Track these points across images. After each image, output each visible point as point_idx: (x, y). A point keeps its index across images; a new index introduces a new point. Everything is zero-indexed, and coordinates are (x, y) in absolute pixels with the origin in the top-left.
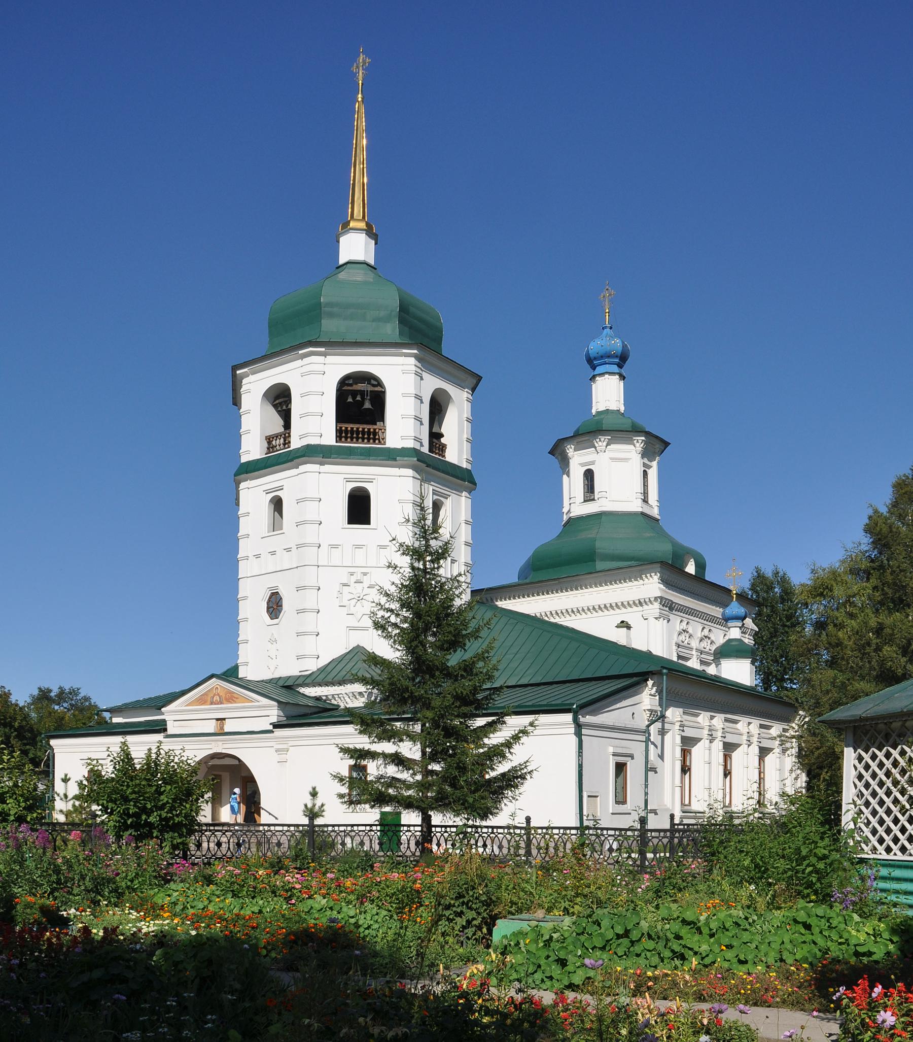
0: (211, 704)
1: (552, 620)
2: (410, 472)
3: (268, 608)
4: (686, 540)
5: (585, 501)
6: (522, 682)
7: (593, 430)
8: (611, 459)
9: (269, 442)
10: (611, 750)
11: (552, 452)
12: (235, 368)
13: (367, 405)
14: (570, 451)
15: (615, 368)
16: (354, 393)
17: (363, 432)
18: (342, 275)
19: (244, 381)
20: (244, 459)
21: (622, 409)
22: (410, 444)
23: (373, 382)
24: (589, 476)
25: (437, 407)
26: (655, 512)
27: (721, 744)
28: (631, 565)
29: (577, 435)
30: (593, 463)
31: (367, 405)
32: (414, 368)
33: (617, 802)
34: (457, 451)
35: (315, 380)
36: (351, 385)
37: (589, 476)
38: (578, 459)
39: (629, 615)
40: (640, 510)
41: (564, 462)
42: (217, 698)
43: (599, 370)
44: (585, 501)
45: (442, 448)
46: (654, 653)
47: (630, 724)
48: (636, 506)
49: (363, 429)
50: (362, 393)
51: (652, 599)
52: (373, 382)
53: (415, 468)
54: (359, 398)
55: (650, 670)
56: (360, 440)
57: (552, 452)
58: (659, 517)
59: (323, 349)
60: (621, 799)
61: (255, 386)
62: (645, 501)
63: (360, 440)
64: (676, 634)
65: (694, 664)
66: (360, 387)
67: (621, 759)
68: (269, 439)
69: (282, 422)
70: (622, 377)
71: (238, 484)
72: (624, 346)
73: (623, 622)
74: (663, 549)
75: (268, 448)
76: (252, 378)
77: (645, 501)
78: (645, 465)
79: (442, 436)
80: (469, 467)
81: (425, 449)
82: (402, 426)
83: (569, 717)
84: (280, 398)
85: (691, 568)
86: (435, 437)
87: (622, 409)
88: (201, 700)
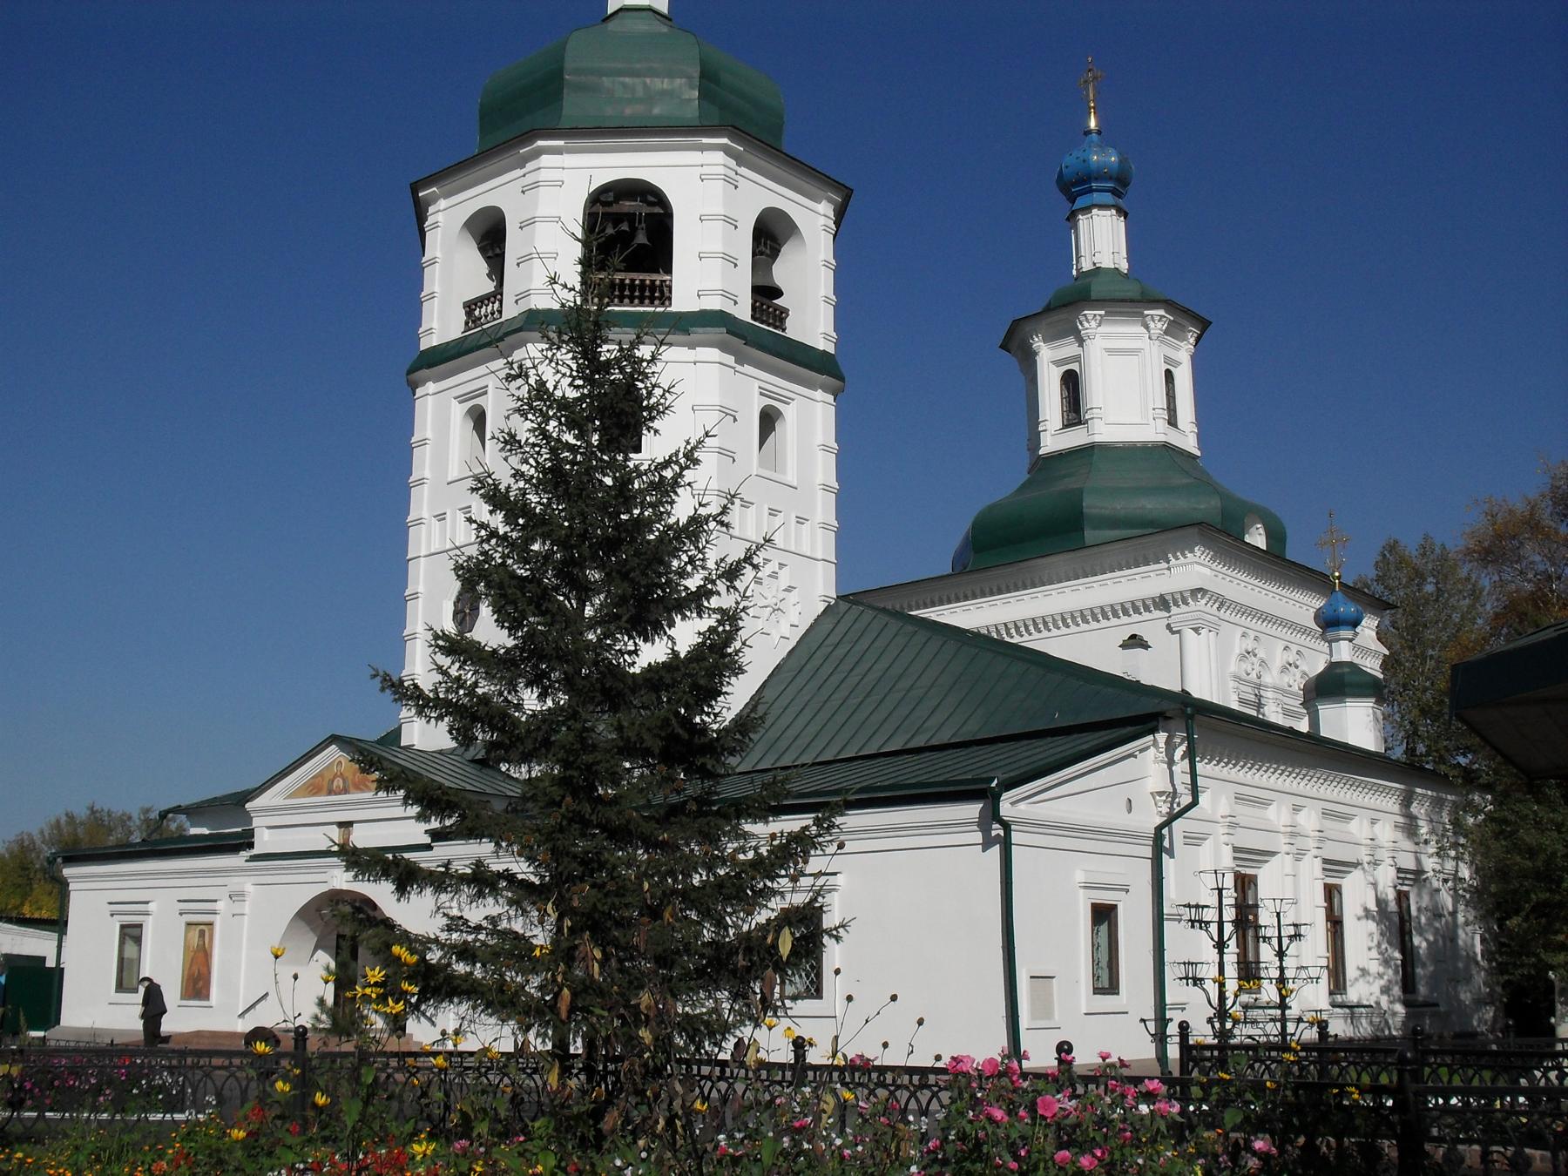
0: (330, 793)
1: (1016, 640)
2: (714, 354)
3: (456, 613)
4: (1244, 491)
5: (1065, 426)
6: (934, 742)
7: (1074, 298)
8: (1107, 350)
9: (469, 313)
10: (1080, 877)
11: (1004, 346)
12: (415, 188)
13: (641, 238)
14: (1038, 343)
15: (1108, 198)
16: (617, 219)
17: (632, 286)
18: (612, 26)
19: (431, 210)
20: (424, 345)
21: (1124, 266)
22: (714, 304)
23: (651, 199)
24: (1071, 382)
25: (770, 235)
26: (1188, 441)
27: (1318, 863)
28: (1151, 536)
29: (1049, 309)
30: (1077, 359)
31: (641, 238)
32: (721, 170)
33: (1338, 888)
34: (812, 319)
35: (549, 194)
36: (609, 204)
37: (1071, 382)
38: (1049, 359)
39: (1151, 626)
40: (1162, 438)
41: (1028, 360)
42: (339, 782)
43: (1080, 202)
44: (1065, 426)
45: (779, 317)
46: (1195, 694)
47: (1116, 818)
48: (1153, 431)
49: (633, 280)
50: (630, 218)
51: (1187, 594)
52: (651, 199)
53: (724, 348)
54: (625, 227)
55: (1158, 709)
56: (626, 301)
57: (1004, 346)
58: (1198, 453)
59: (561, 143)
60: (1107, 982)
61: (448, 216)
62: (1172, 422)
63: (626, 301)
64: (1234, 659)
65: (1273, 715)
66: (627, 206)
67: (1106, 897)
68: (470, 307)
69: (483, 267)
70: (1121, 212)
71: (414, 386)
72: (1122, 162)
73: (1133, 637)
74: (1207, 506)
75: (467, 323)
76: (442, 203)
77: (1172, 422)
78: (1167, 360)
79: (778, 293)
80: (831, 349)
81: (743, 312)
82: (705, 270)
83: (972, 810)
84: (490, 235)
85: (1257, 538)
86: (765, 293)
87: (1124, 266)
88: (314, 787)
